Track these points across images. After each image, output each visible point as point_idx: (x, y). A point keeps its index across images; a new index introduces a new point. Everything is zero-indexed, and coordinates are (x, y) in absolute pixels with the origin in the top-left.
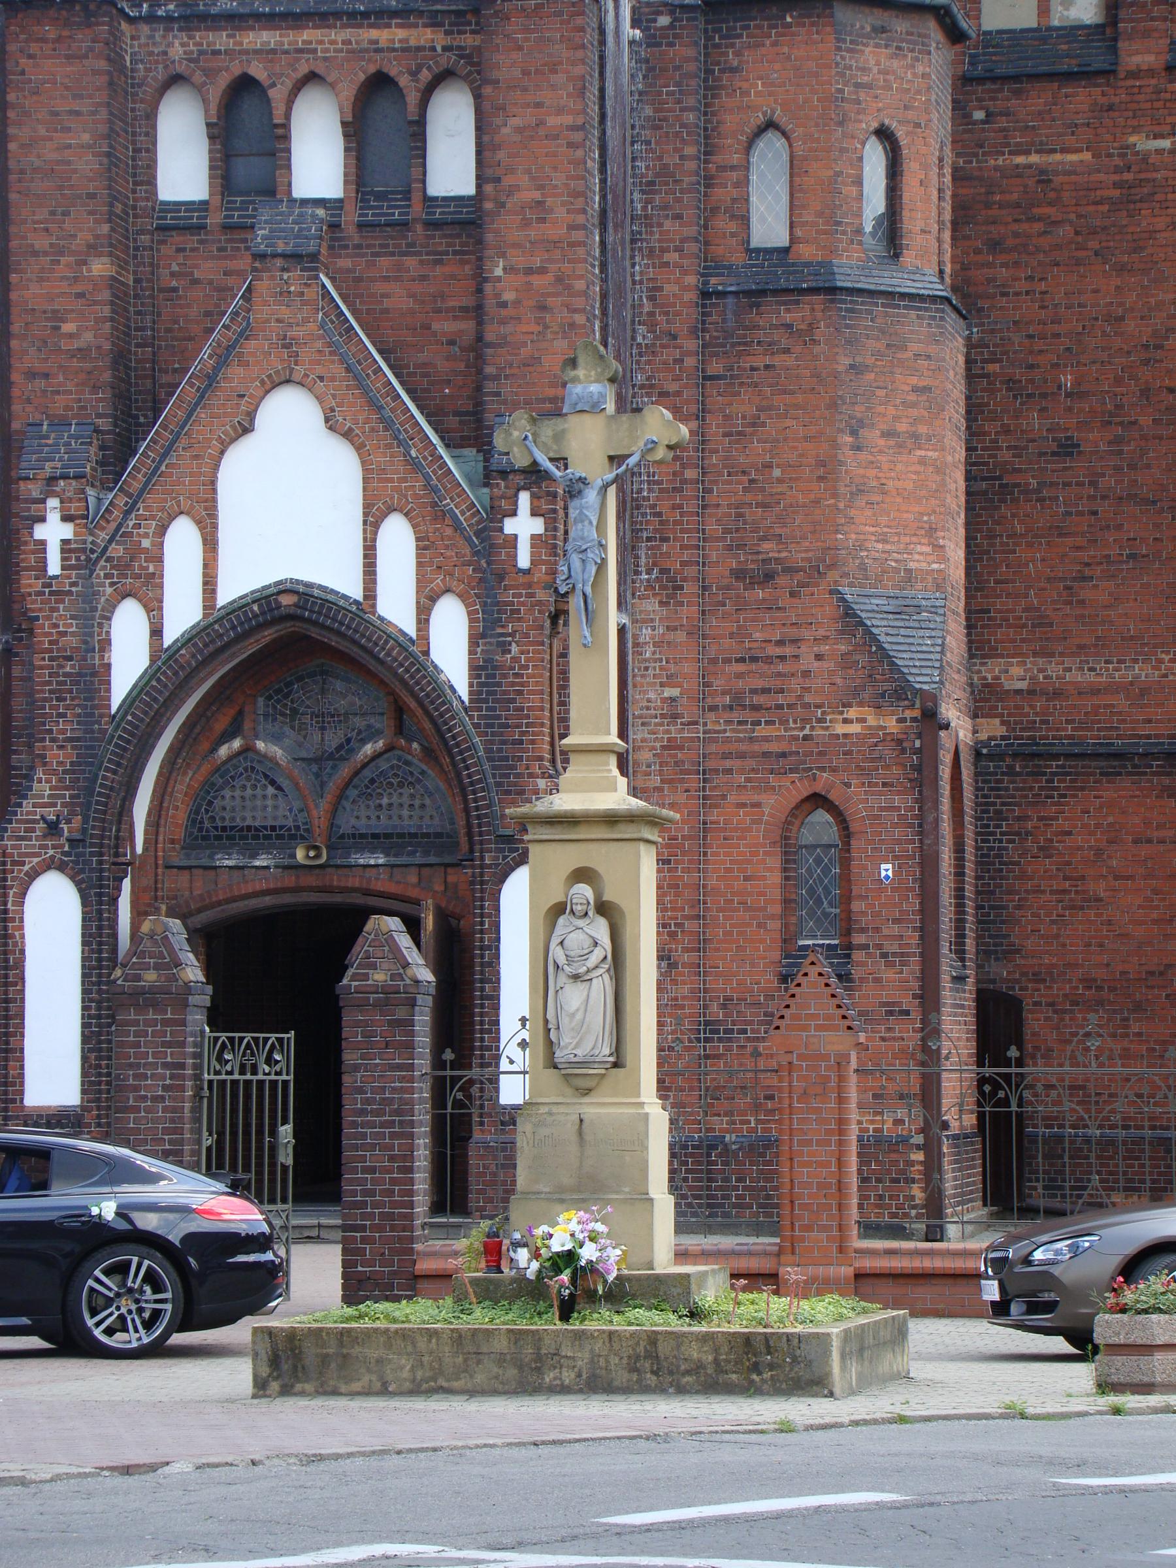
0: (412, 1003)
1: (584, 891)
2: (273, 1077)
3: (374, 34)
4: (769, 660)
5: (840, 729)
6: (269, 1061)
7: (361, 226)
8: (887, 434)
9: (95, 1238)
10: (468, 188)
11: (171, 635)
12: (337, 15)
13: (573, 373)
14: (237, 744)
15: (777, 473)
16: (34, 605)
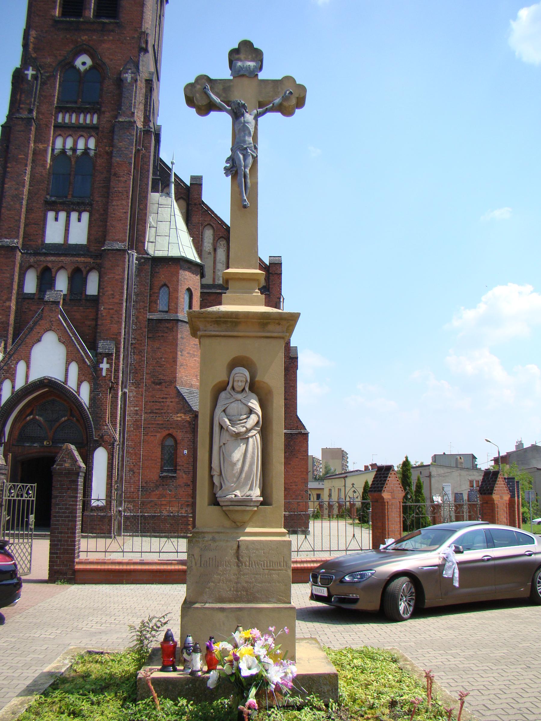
0: (78, 474)
1: (242, 375)
2: (28, 499)
3: (77, 259)
4: (160, 402)
5: (176, 419)
6: (28, 493)
7: (70, 300)
8: (188, 353)
10: (96, 293)
12: (69, 254)
13: (237, 56)
14: (31, 417)
15: (163, 360)
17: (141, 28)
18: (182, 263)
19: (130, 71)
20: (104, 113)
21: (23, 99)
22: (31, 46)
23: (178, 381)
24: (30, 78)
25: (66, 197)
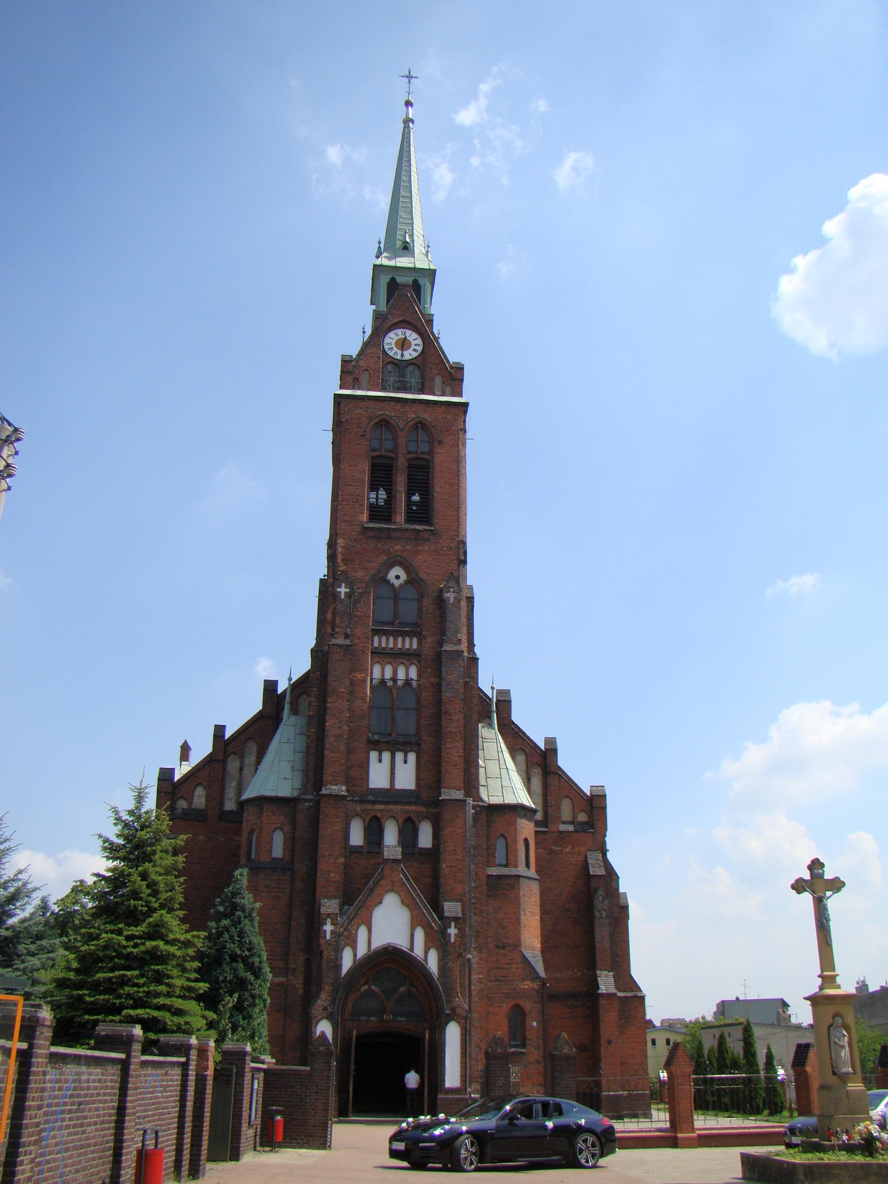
1: (839, 1020)
4: (504, 969)
9: (580, 1129)
11: (359, 955)
16: (323, 947)
17: (458, 536)
18: (519, 810)
19: (451, 590)
20: (425, 637)
21: (337, 621)
22: (339, 557)
23: (523, 944)
24: (343, 597)
25: (390, 735)
